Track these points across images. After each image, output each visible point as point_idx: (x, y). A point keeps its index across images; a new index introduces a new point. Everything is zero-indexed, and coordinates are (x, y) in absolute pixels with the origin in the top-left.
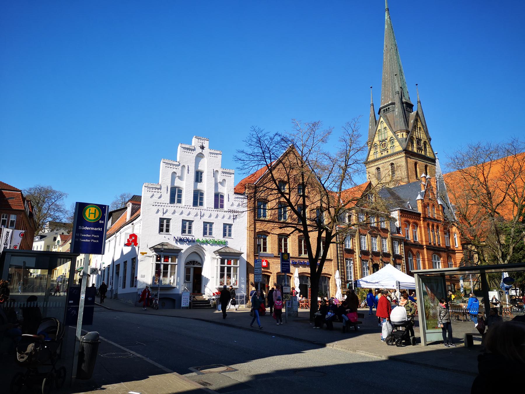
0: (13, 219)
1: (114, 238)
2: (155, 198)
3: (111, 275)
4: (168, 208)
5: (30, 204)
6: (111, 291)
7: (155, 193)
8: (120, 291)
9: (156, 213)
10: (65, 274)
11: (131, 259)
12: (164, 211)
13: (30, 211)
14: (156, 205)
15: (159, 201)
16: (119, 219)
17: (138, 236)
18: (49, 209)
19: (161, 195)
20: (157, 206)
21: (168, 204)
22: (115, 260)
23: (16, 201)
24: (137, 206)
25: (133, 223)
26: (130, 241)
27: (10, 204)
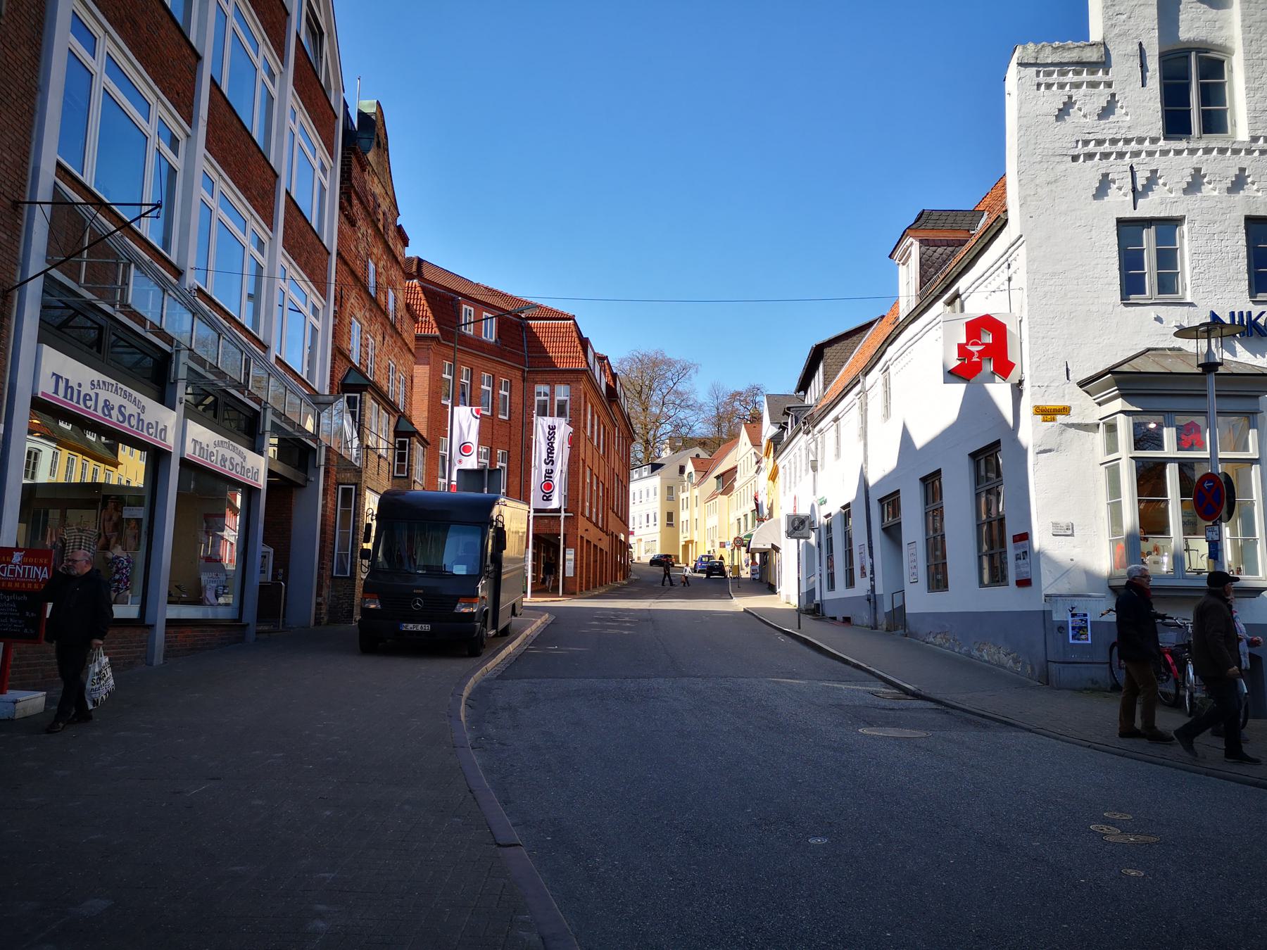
0: (563, 398)
1: (857, 401)
2: (1083, 120)
3: (859, 539)
4: (1158, 162)
5: (607, 367)
6: (869, 600)
7: (1078, 94)
8: (828, 596)
9: (1096, 197)
10: (712, 552)
11: (967, 458)
12: (1141, 182)
13: (607, 385)
14: (1090, 156)
15: (1107, 129)
16: (847, 365)
17: (1011, 328)
18: (663, 404)
19: (1113, 95)
20: (1098, 156)
21: (1154, 141)
22: (872, 481)
23: (557, 332)
24: (940, 250)
25: (958, 290)
26: (972, 354)
27: (551, 354)
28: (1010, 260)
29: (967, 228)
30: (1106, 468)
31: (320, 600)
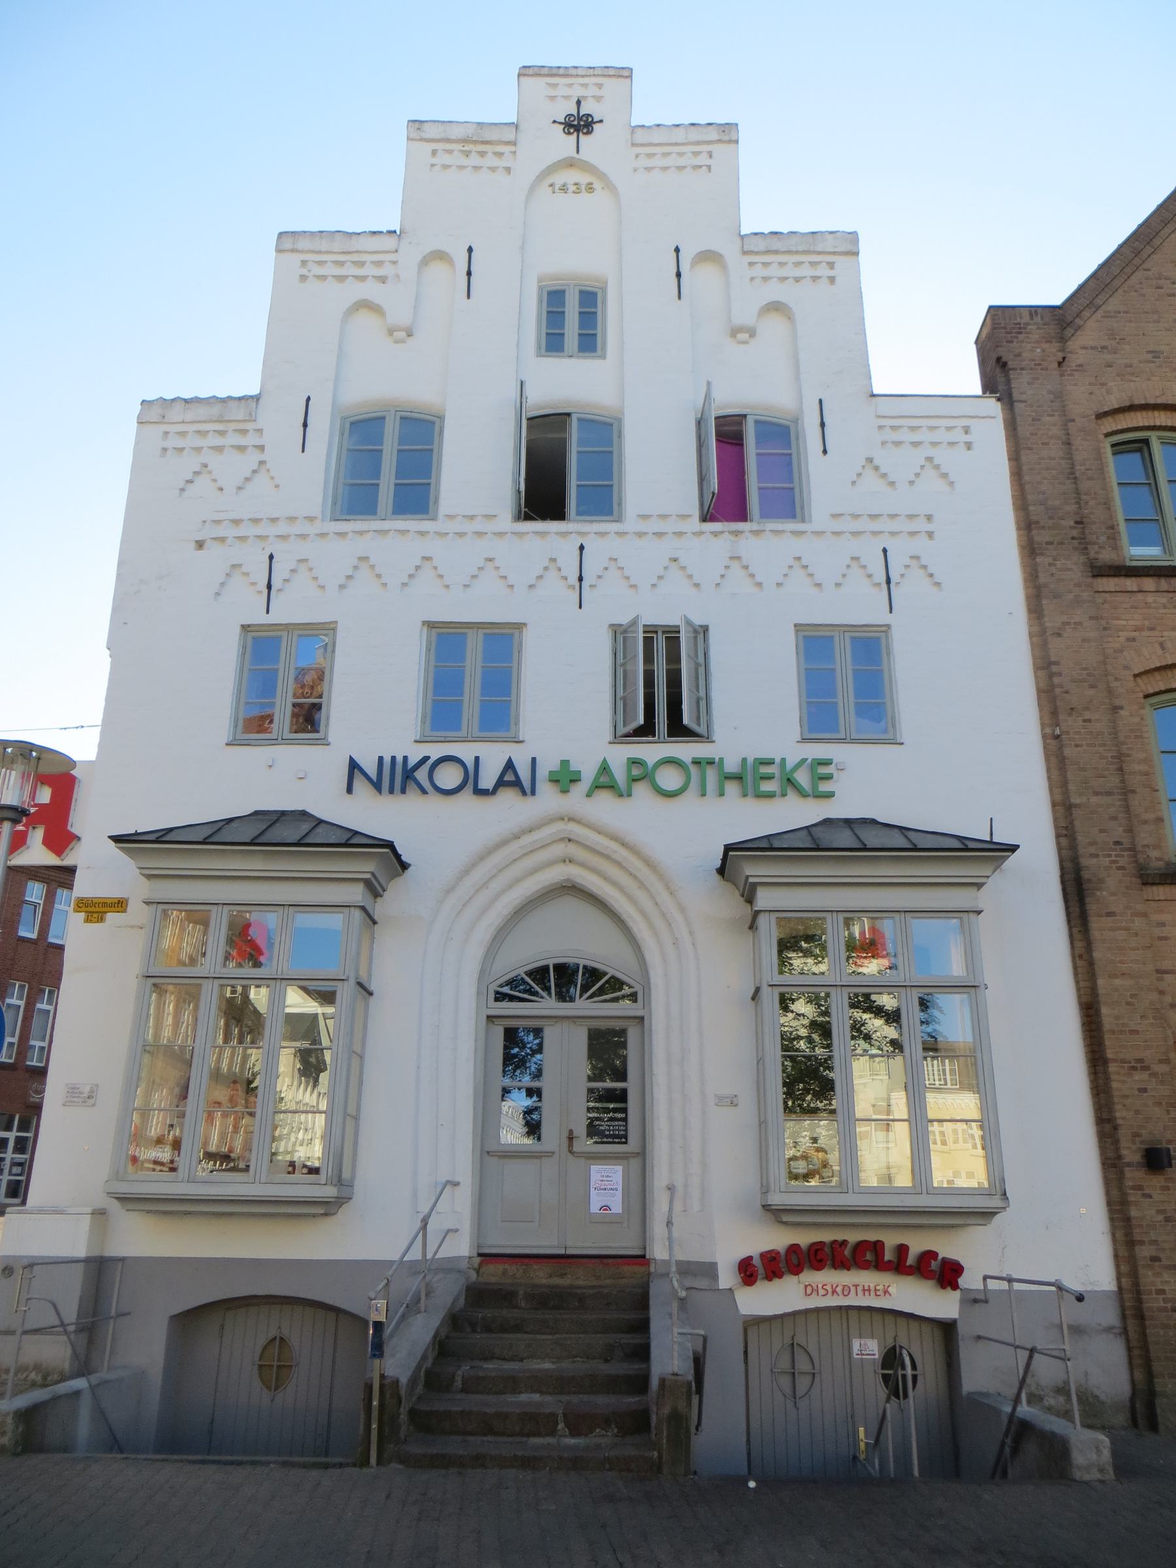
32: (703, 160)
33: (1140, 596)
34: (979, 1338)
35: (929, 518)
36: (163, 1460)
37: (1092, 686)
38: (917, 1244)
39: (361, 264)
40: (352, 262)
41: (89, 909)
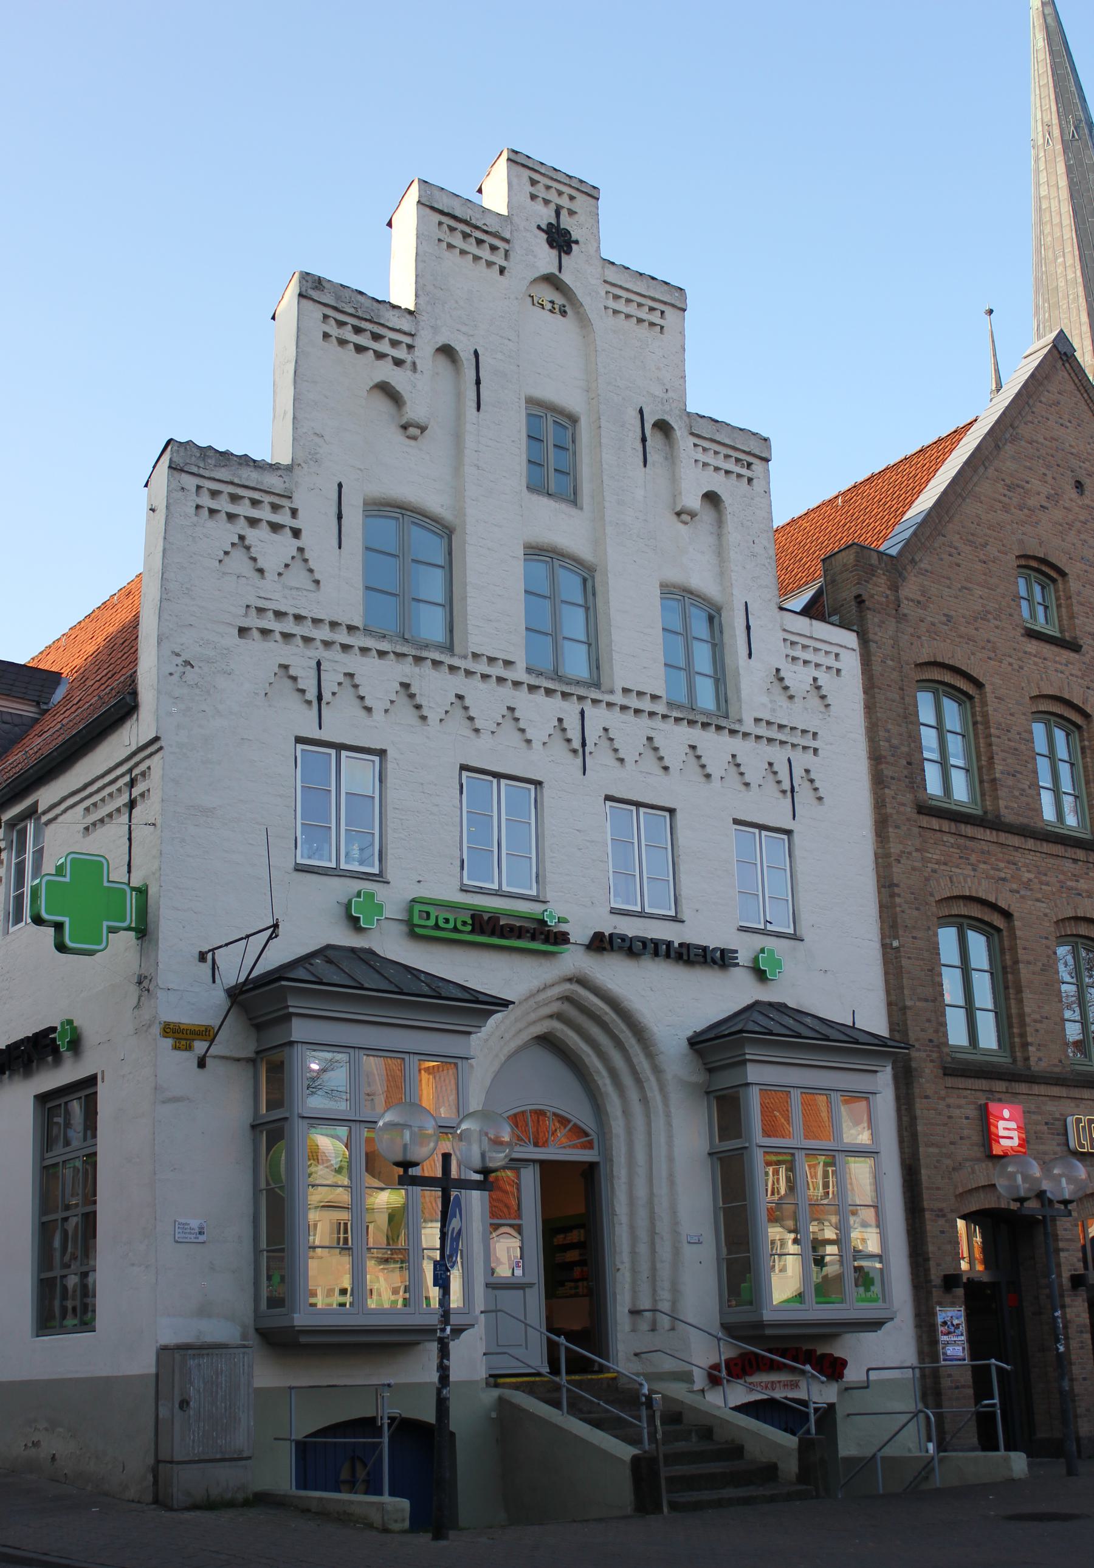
25: (36, 804)
28: (135, 772)
29: (36, 699)
30: (760, 1090)
31: (407, 1295)
32: (655, 318)
33: (939, 835)
34: (849, 1415)
35: (815, 734)
36: (19, 1549)
37: (917, 909)
38: (806, 1347)
39: (377, 337)
40: (335, 320)
41: (177, 1035)
